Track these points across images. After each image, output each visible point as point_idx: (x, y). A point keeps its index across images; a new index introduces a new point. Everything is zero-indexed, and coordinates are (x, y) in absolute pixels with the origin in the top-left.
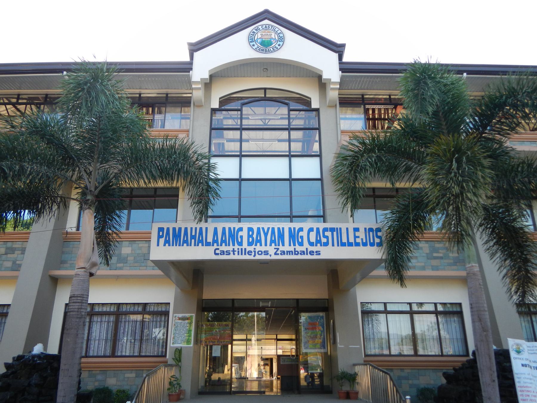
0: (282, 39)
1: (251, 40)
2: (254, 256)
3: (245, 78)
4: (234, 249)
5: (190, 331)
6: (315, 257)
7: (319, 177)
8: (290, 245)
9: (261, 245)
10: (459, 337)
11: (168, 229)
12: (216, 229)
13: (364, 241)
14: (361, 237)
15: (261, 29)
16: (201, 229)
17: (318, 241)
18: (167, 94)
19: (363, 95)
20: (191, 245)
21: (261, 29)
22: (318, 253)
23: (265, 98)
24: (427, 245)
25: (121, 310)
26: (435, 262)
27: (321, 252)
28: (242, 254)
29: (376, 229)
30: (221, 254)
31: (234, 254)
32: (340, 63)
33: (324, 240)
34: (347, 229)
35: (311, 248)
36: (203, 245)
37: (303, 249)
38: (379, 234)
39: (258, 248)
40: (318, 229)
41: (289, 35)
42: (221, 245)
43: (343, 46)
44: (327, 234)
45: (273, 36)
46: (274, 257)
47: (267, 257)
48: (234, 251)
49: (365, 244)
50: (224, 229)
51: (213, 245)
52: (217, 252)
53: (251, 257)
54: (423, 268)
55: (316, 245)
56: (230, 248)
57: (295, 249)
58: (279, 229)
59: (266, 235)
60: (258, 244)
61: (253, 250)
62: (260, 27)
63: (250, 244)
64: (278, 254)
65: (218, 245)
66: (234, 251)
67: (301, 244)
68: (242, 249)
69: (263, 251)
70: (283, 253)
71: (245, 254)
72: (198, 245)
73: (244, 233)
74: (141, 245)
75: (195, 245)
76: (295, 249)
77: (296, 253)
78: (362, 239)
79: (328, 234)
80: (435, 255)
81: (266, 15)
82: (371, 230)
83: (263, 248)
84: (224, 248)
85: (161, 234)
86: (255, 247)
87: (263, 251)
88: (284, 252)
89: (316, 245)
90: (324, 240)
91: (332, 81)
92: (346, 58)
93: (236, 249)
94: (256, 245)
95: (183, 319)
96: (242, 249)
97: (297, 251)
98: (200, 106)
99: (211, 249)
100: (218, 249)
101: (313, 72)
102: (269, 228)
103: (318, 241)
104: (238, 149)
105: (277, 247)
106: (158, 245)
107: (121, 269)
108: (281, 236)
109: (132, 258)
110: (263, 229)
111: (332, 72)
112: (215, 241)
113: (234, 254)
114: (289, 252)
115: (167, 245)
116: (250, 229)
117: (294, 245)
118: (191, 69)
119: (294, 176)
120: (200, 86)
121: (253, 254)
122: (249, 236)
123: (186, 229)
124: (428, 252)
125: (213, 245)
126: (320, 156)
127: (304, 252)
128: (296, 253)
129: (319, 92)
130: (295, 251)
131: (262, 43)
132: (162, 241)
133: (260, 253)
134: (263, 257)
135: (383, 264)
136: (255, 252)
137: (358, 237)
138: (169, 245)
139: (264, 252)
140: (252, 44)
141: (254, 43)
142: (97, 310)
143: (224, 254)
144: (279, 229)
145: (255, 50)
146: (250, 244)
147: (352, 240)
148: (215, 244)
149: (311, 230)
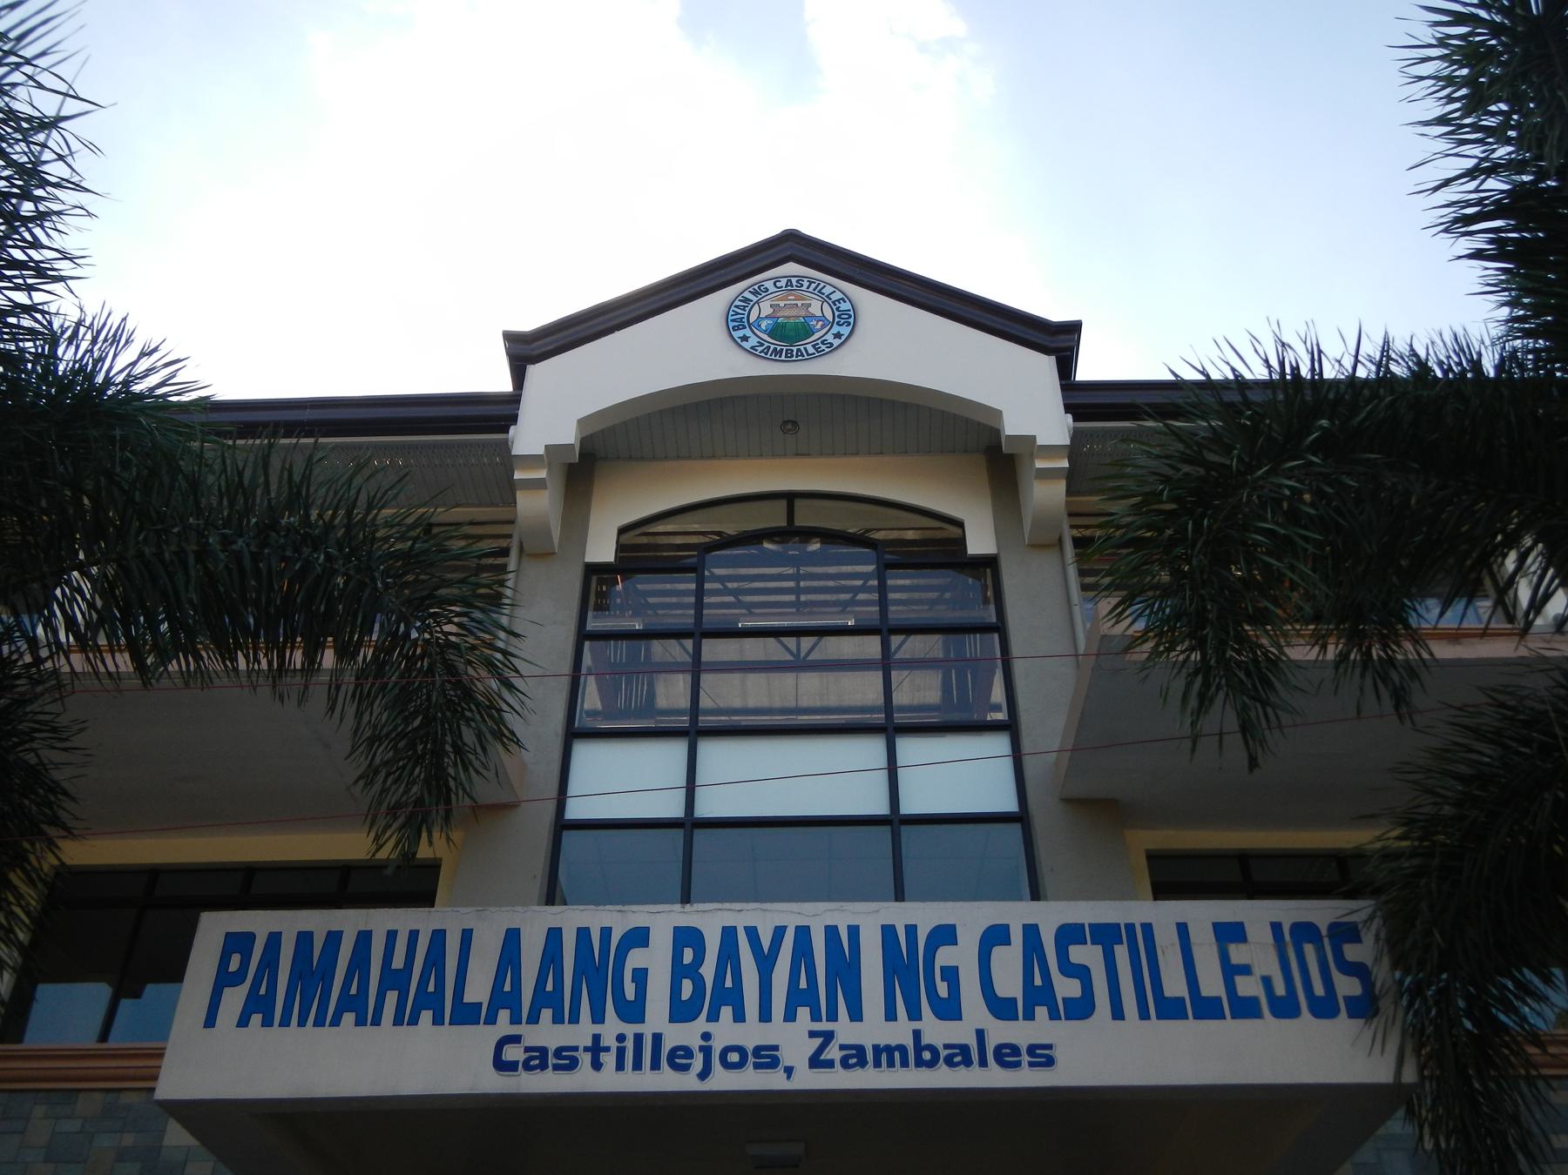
0: (848, 318)
1: (736, 323)
2: (704, 1074)
3: (716, 462)
4: (596, 1038)
6: (1026, 1077)
7: (1009, 804)
8: (891, 1015)
9: (739, 1017)
11: (274, 939)
12: (512, 938)
13: (1280, 990)
14: (1259, 971)
15: (772, 289)
16: (439, 937)
17: (1038, 995)
20: (376, 1022)
21: (772, 289)
22: (1042, 1056)
23: (791, 526)
27: (1057, 1053)
28: (637, 1066)
29: (1333, 927)
30: (527, 1067)
31: (597, 1065)
32: (1064, 388)
33: (1067, 988)
35: (1001, 1032)
38: (1352, 952)
39: (726, 1032)
40: (1031, 932)
42: (534, 1019)
43: (1074, 328)
44: (1078, 954)
45: (815, 309)
46: (808, 1080)
47: (773, 1081)
48: (596, 1048)
49: (1285, 1008)
50: (554, 935)
52: (513, 1053)
53: (688, 1082)
55: (1029, 1016)
56: (579, 1034)
57: (917, 1034)
58: (831, 931)
59: (765, 963)
60: (726, 1012)
61: (695, 1043)
62: (769, 285)
63: (681, 1012)
64: (830, 1064)
65: (516, 1020)
66: (596, 1048)
67: (949, 1010)
68: (639, 1038)
69: (750, 1047)
71: (655, 1065)
72: (414, 1021)
73: (656, 959)
75: (398, 1021)
76: (917, 1034)
77: (925, 1055)
78: (1267, 982)
79: (1087, 954)
83: (751, 1034)
84: (547, 1034)
85: (235, 964)
86: (710, 1027)
87: (750, 1047)
88: (860, 1050)
89: (1029, 1016)
90: (1067, 988)
91: (1039, 442)
92: (1088, 369)
93: (609, 1040)
94: (713, 1017)
96: (639, 1038)
97: (931, 1048)
98: (546, 555)
99: (482, 1039)
100: (516, 1039)
101: (967, 421)
102: (779, 932)
103: (1038, 995)
104: (684, 702)
105: (824, 1026)
106: (210, 1022)
108: (845, 968)
110: (752, 933)
112: (505, 999)
113: (597, 1065)
114: (887, 1055)
115: (256, 1019)
116: (687, 937)
117: (914, 1014)
118: (514, 419)
119: (908, 807)
120: (542, 474)
121: (698, 1063)
122: (680, 971)
126: (1010, 727)
127: (964, 1049)
128: (925, 1055)
129: (994, 506)
130: (919, 1048)
131: (778, 332)
132: (234, 998)
133: (734, 1057)
134: (750, 1080)
135: (1397, 1125)
136: (707, 1051)
137: (1246, 970)
139: (758, 1050)
140: (737, 334)
141: (747, 332)
143: (543, 1066)
144: (831, 931)
145: (752, 352)
146: (681, 1012)
148: (504, 1015)
149: (995, 936)
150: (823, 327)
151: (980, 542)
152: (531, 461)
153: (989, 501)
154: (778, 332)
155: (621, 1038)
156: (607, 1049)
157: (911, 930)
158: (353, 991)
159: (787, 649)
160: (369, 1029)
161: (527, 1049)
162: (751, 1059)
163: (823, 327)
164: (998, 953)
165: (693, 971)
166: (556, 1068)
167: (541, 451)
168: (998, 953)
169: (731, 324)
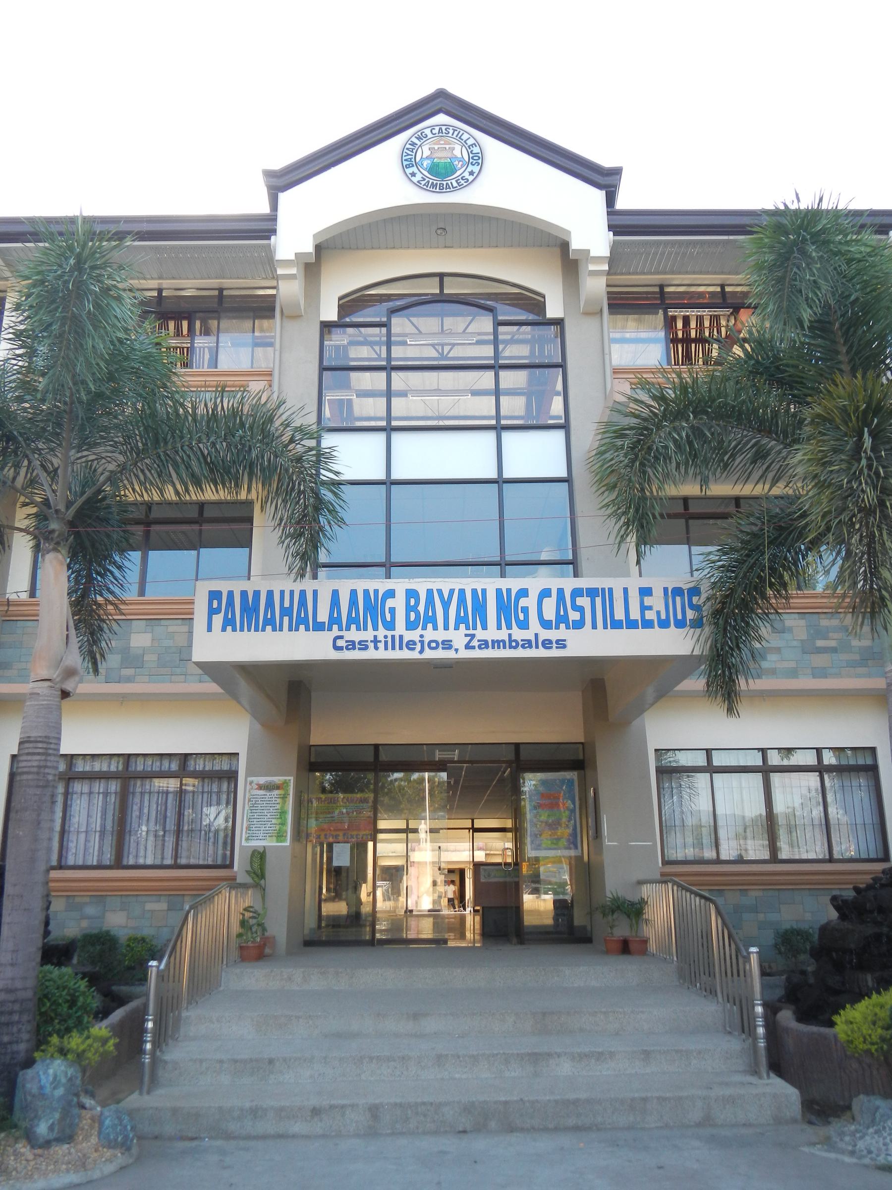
0: (477, 159)
1: (408, 161)
2: (421, 652)
4: (375, 637)
5: (283, 813)
6: (555, 653)
7: (563, 474)
8: (499, 628)
9: (435, 628)
10: (868, 820)
13: (663, 617)
14: (655, 609)
15: (430, 135)
17: (562, 619)
18: (221, 290)
19: (662, 287)
20: (281, 630)
22: (561, 644)
24: (802, 623)
25: (132, 768)
26: (820, 660)
28: (393, 648)
30: (347, 649)
31: (376, 648)
32: (609, 213)
33: (574, 616)
34: (626, 590)
35: (545, 634)
36: (307, 629)
37: (528, 635)
39: (430, 634)
40: (561, 591)
41: (491, 146)
42: (348, 629)
43: (616, 172)
45: (457, 152)
46: (464, 654)
47: (450, 654)
48: (376, 641)
49: (664, 624)
50: (354, 593)
51: (330, 629)
52: (340, 643)
53: (414, 655)
54: (793, 673)
55: (557, 628)
56: (368, 635)
57: (510, 635)
58: (474, 591)
59: (446, 605)
60: (430, 626)
62: (428, 131)
63: (411, 626)
64: (473, 648)
65: (340, 629)
66: (376, 641)
67: (524, 625)
68: (393, 637)
70: (484, 644)
71: (401, 648)
72: (297, 629)
73: (398, 603)
74: (171, 629)
75: (290, 629)
76: (510, 635)
77: (513, 644)
78: (658, 613)
80: (820, 643)
81: (442, 102)
82: (678, 591)
83: (440, 635)
84: (354, 635)
86: (423, 632)
88: (486, 642)
89: (557, 628)
90: (574, 616)
91: (592, 254)
92: (621, 204)
93: (381, 637)
94: (424, 628)
95: (269, 787)
96: (393, 637)
97: (515, 641)
98: (296, 317)
99: (327, 637)
100: (341, 637)
101: (550, 234)
102: (452, 592)
103: (562, 619)
105: (471, 632)
106: (209, 629)
107: (129, 680)
108: (480, 607)
109: (154, 657)
110: (440, 592)
111: (592, 237)
112: (335, 620)
113: (376, 648)
114: (497, 644)
115: (229, 628)
116: (411, 594)
117: (509, 627)
118: (274, 231)
119: (507, 475)
120: (294, 271)
122: (409, 609)
123: (270, 594)
124: (804, 637)
125: (330, 629)
126: (565, 427)
127: (529, 641)
128: (513, 644)
129: (563, 282)
132: (218, 620)
133: (433, 645)
136: (422, 642)
137: (650, 608)
138: (234, 630)
140: (409, 171)
141: (414, 169)
142: (81, 770)
143: (354, 648)
144: (474, 591)
145: (418, 185)
146: (411, 626)
147: (635, 614)
148: (335, 627)
149: (545, 593)
150: (462, 166)
151: (553, 311)
152: (286, 263)
153: (560, 272)
154: (434, 170)
155: (386, 637)
156: (380, 641)
157: (509, 591)
158: (269, 616)
159: (437, 351)
160: (278, 632)
161: (347, 641)
162: (441, 646)
163: (462, 166)
164: (546, 600)
165: (415, 608)
166: (359, 649)
167: (293, 257)
168: (546, 600)
169: (405, 163)
